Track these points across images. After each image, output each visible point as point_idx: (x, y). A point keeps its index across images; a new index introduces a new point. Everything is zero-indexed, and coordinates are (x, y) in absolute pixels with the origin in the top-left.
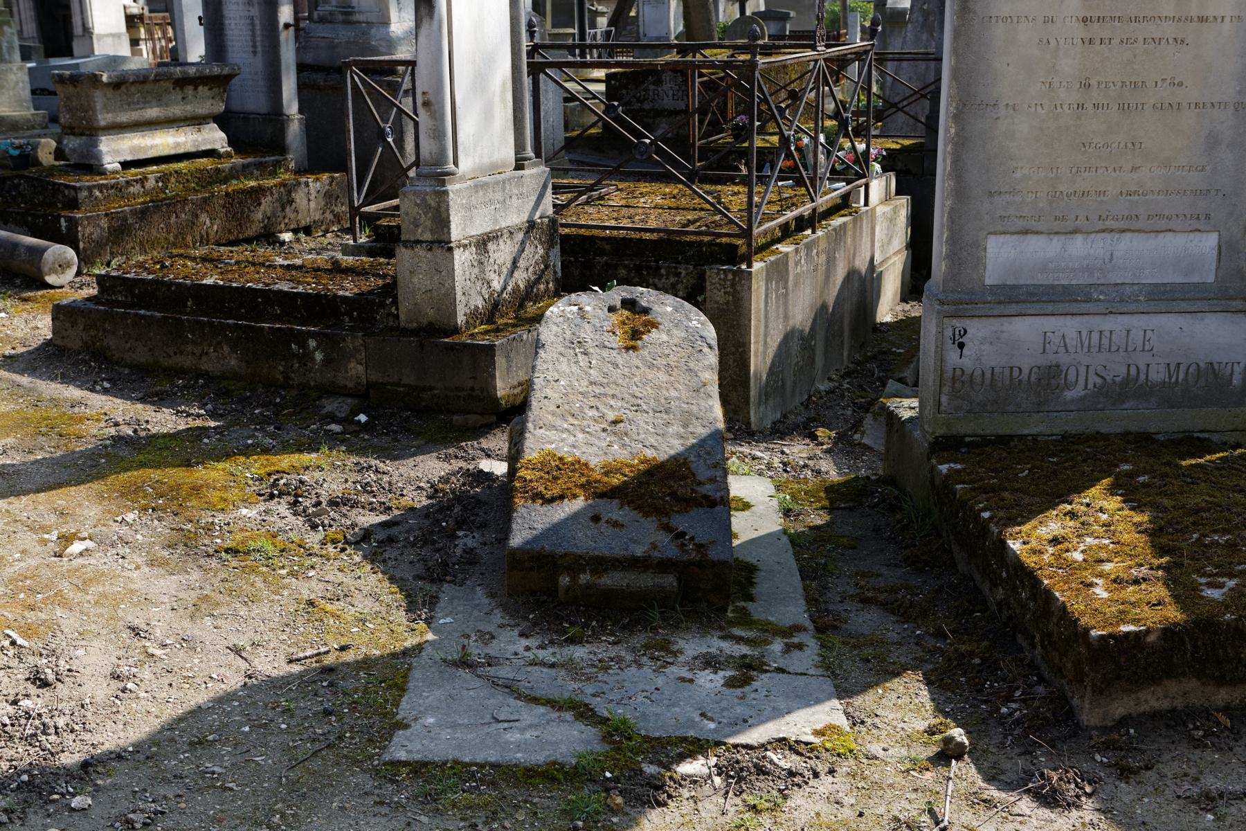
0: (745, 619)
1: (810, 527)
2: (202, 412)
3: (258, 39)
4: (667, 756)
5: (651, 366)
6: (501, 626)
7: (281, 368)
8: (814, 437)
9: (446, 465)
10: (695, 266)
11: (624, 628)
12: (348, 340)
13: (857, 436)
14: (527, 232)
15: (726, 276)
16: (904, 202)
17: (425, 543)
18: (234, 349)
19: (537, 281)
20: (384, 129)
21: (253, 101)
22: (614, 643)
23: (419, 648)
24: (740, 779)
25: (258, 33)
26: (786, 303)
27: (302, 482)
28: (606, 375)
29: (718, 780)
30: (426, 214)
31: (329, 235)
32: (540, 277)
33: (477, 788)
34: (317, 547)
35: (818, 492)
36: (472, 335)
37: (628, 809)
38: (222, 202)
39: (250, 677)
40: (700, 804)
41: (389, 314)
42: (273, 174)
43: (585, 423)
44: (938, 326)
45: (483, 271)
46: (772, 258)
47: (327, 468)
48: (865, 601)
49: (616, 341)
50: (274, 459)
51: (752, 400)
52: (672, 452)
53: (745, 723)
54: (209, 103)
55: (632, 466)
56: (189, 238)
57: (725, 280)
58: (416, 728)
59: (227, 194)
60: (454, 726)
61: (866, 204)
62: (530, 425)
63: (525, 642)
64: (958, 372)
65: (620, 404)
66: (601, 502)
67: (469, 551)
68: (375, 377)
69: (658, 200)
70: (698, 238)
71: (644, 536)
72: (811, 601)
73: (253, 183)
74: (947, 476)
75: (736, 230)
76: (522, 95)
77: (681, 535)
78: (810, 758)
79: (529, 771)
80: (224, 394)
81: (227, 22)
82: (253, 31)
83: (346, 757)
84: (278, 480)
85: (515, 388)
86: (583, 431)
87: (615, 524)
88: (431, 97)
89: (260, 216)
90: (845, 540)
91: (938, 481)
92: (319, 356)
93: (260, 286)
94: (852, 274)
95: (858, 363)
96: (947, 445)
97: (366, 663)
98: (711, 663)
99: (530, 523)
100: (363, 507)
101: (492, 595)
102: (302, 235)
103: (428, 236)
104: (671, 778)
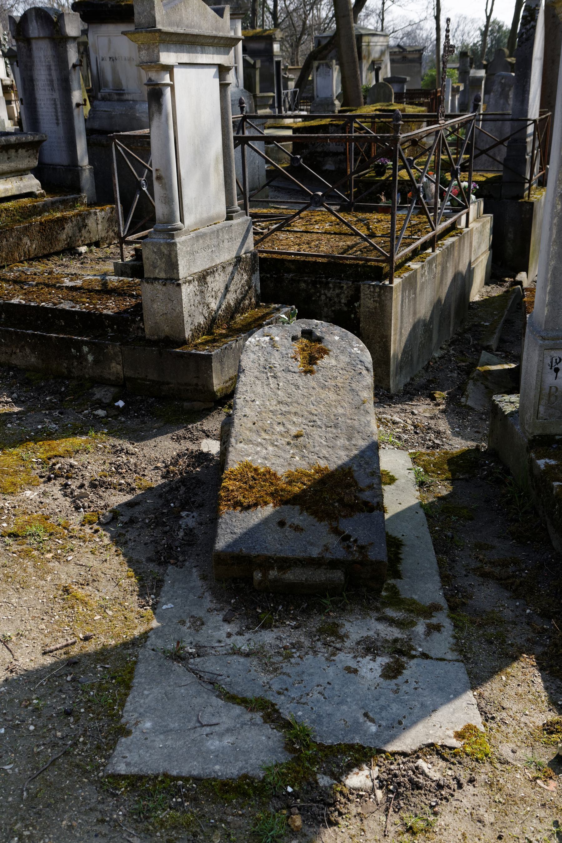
0: (396, 600)
1: (439, 498)
2: (10, 400)
3: (59, 114)
4: (338, 766)
5: (324, 387)
6: (209, 611)
7: (65, 365)
8: (433, 399)
9: (177, 445)
11: (303, 611)
12: (110, 347)
13: (463, 400)
14: (235, 265)
15: (375, 289)
16: (488, 219)
17: (157, 525)
19: (243, 299)
20: (140, 182)
21: (58, 157)
22: (296, 628)
23: (145, 636)
24: (398, 795)
25: (59, 110)
26: (415, 304)
27: (72, 466)
28: (290, 395)
29: (379, 794)
31: (111, 246)
32: (246, 295)
33: (181, 804)
34: (78, 527)
35: (442, 465)
36: (196, 346)
37: (306, 829)
38: (37, 229)
39: (12, 672)
40: (365, 822)
41: (139, 328)
42: (73, 207)
43: (274, 437)
44: (540, 356)
45: (204, 298)
46: (406, 275)
47: (91, 450)
48: (485, 575)
49: (297, 366)
50: (55, 443)
51: (391, 373)
52: (340, 462)
53: (399, 726)
54: (27, 161)
55: (310, 476)
56: (16, 255)
57: (374, 292)
58: (136, 733)
59: (41, 223)
60: (166, 732)
61: (467, 226)
62: (233, 440)
63: (228, 628)
64: (553, 390)
65: (300, 420)
66: (286, 508)
67: (189, 532)
69: (327, 226)
70: (356, 262)
71: (318, 540)
72: (445, 579)
73: (59, 215)
74: (545, 473)
75: (382, 258)
76: (230, 164)
77: (347, 538)
78: (453, 764)
79: (225, 785)
80: (27, 383)
81: (38, 102)
82: (56, 109)
83: (78, 766)
84: (54, 464)
85: (227, 382)
86: (273, 445)
87: (297, 528)
88: (163, 175)
89: (64, 237)
90: (465, 511)
91: (536, 472)
92: (90, 358)
93: (50, 305)
94: (457, 275)
95: (459, 334)
96: (543, 443)
97: (103, 655)
98: (370, 648)
99: (233, 527)
100: (115, 488)
101: (204, 578)
102: (93, 248)
103: (163, 275)
104: (341, 793)
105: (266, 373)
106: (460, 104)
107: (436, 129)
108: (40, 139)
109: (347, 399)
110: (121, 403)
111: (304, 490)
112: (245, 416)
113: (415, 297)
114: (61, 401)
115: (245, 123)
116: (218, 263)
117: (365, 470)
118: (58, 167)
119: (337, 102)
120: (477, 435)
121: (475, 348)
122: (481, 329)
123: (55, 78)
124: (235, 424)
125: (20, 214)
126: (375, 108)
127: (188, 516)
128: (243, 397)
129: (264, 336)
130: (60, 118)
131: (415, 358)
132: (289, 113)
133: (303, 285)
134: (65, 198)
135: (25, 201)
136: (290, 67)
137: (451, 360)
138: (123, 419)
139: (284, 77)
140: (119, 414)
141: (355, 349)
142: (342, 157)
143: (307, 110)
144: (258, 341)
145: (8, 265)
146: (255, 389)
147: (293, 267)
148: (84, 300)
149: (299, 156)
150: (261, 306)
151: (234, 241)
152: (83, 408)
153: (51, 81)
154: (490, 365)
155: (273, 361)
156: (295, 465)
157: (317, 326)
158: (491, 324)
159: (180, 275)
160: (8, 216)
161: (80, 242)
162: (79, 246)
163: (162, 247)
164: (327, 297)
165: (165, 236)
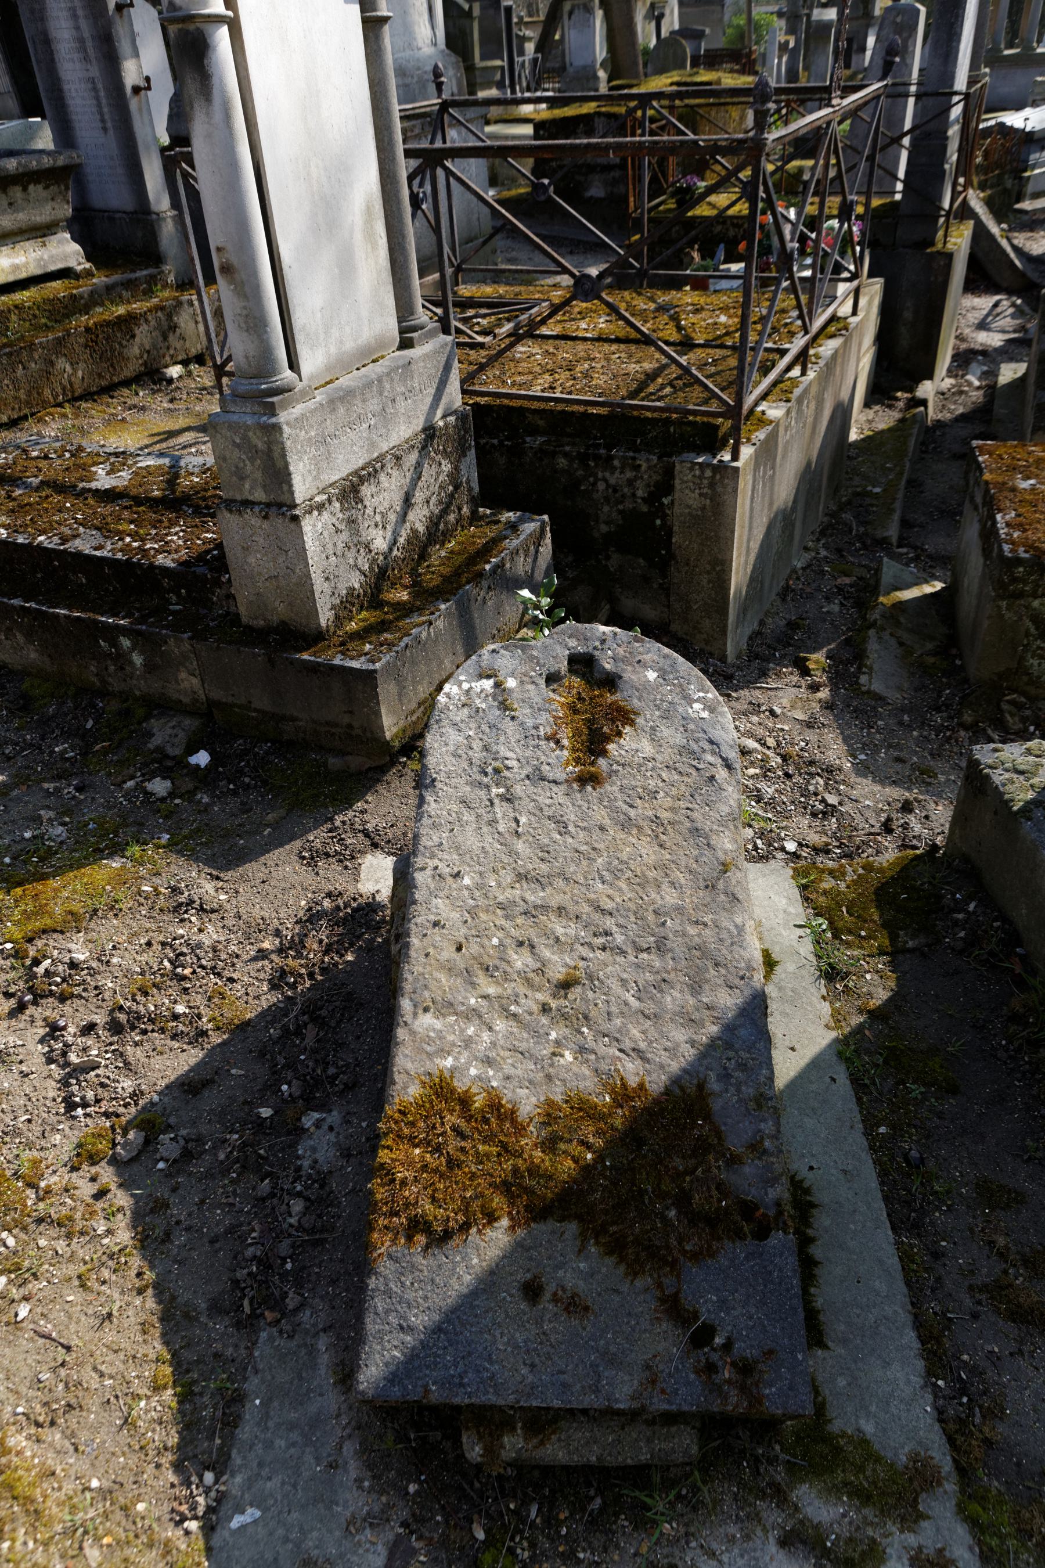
3: (106, 110)
5: (626, 824)
6: (352, 1526)
7: (92, 668)
10: (660, 458)
12: (171, 642)
14: (424, 447)
15: (703, 472)
18: (29, 635)
19: (445, 512)
25: (104, 101)
28: (545, 853)
30: (252, 460)
32: (449, 505)
38: (82, 340)
42: (149, 293)
45: (358, 533)
49: (559, 762)
51: (730, 627)
52: (675, 1066)
54: (48, 207)
56: (47, 393)
59: (88, 329)
62: (406, 1005)
66: (543, 1229)
68: (217, 694)
73: (121, 310)
81: (66, 87)
82: (97, 98)
85: (413, 712)
87: (574, 1305)
88: (234, 260)
89: (136, 351)
95: (832, 515)
102: (193, 367)
103: (259, 495)
105: (488, 787)
106: (788, 71)
107: (827, 119)
108: (67, 161)
109: (683, 861)
110: (202, 758)
111: (587, 1170)
112: (436, 924)
114: (84, 754)
115: (446, 116)
117: (739, 1090)
118: (118, 215)
119: (602, 74)
120: (899, 766)
121: (864, 543)
122: (868, 501)
123: (87, 34)
124: (413, 953)
125: (47, 314)
126: (669, 81)
127: (318, 1124)
128: (431, 863)
129: (481, 676)
130: (107, 117)
131: (767, 585)
132: (527, 95)
133: (562, 462)
134: (133, 276)
135: (56, 285)
136: (526, 19)
137: (822, 573)
138: (206, 799)
139: (518, 36)
140: (196, 788)
142: (616, 174)
143: (553, 90)
144: (468, 692)
145: (32, 414)
146: (460, 839)
148: (123, 527)
149: (546, 181)
151: (424, 392)
152: (125, 772)
153: (81, 41)
154: (900, 589)
155: (503, 751)
156: (564, 1081)
157: (603, 641)
158: (884, 490)
160: (24, 320)
161: (168, 358)
162: (167, 367)
163: (251, 434)
164: (608, 486)
165: (256, 408)
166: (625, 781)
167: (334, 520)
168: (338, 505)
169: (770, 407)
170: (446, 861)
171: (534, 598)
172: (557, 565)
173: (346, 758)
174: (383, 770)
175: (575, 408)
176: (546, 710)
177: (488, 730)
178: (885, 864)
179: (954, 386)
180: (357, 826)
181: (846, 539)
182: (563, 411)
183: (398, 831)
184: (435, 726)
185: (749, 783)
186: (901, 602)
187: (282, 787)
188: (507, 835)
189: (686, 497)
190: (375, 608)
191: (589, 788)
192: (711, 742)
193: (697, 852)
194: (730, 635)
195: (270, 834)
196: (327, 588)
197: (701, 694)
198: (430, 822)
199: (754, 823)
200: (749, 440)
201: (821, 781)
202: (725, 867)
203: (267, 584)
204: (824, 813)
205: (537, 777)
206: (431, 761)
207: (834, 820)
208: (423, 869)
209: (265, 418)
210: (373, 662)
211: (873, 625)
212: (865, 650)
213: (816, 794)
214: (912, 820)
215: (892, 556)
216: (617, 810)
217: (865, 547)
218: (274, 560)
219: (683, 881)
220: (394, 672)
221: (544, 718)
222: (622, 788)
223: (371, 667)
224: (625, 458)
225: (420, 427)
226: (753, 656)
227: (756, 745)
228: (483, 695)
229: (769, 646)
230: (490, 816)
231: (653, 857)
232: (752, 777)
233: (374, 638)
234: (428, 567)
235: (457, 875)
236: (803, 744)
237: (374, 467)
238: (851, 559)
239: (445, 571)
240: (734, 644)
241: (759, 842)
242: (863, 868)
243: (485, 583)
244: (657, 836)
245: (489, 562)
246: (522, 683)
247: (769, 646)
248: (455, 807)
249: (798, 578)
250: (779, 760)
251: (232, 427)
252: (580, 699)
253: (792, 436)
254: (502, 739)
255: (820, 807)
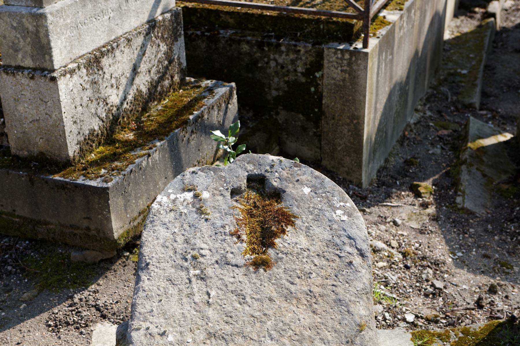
5: (289, 296)
10: (313, 45)
19: (162, 79)
30: (24, 38)
45: (98, 91)
49: (239, 251)
57: (342, 59)
85: (135, 219)
95: (434, 88)
103: (28, 63)
105: (187, 269)
109: (330, 323)
113: (393, 58)
116: (120, 33)
120: (485, 261)
121: (456, 107)
122: (458, 79)
128: (144, 325)
129: (184, 190)
133: (245, 47)
137: (428, 127)
141: (339, 212)
144: (174, 201)
146: (166, 307)
147: (231, 21)
150: (188, 84)
155: (199, 243)
157: (272, 166)
158: (469, 72)
159: (55, 63)
163: (24, 20)
164: (277, 64)
166: (287, 266)
167: (82, 81)
168: (84, 71)
169: (389, 14)
170: (155, 324)
171: (223, 136)
172: (241, 115)
173: (84, 252)
174: (111, 261)
175: (255, 11)
176: (230, 214)
177: (188, 228)
178: (478, 330)
179: (513, 6)
180: (91, 302)
181: (444, 104)
182: (246, 14)
183: (121, 306)
184: (150, 225)
185: (380, 273)
186: (483, 147)
187: (35, 273)
188: (201, 305)
189: (332, 72)
190: (109, 144)
191: (261, 270)
192: (350, 238)
193: (340, 317)
194: (364, 169)
195: (25, 308)
196: (75, 129)
197: (342, 204)
198: (144, 294)
199: (383, 301)
200: (374, 35)
201: (431, 271)
202: (361, 328)
203: (31, 125)
204: (434, 294)
205: (224, 262)
206: (146, 250)
207: (441, 299)
208: (138, 329)
209: (35, 10)
210: (106, 182)
211: (464, 162)
212: (460, 179)
213: (427, 281)
214: (496, 299)
215: (476, 116)
216: (281, 286)
217: (457, 110)
218: (37, 108)
219: (330, 338)
220: (122, 190)
221: (229, 220)
222: (285, 271)
223: (105, 185)
224: (289, 45)
225: (145, 20)
226: (381, 183)
227: (384, 246)
228: (185, 203)
229: (392, 177)
230: (189, 291)
231: (308, 320)
232: (381, 268)
233: (107, 165)
234: (149, 116)
235: (163, 334)
236: (417, 245)
237: (111, 46)
238: (448, 118)
239: (161, 119)
240: (367, 175)
241: (387, 315)
242: (462, 332)
243: (189, 129)
244: (311, 305)
245: (192, 114)
246: (214, 195)
247: (392, 177)
248: (163, 284)
249: (411, 131)
250: (401, 256)
251: (10, 15)
252: (256, 207)
253: (404, 33)
254: (198, 235)
255: (431, 290)
